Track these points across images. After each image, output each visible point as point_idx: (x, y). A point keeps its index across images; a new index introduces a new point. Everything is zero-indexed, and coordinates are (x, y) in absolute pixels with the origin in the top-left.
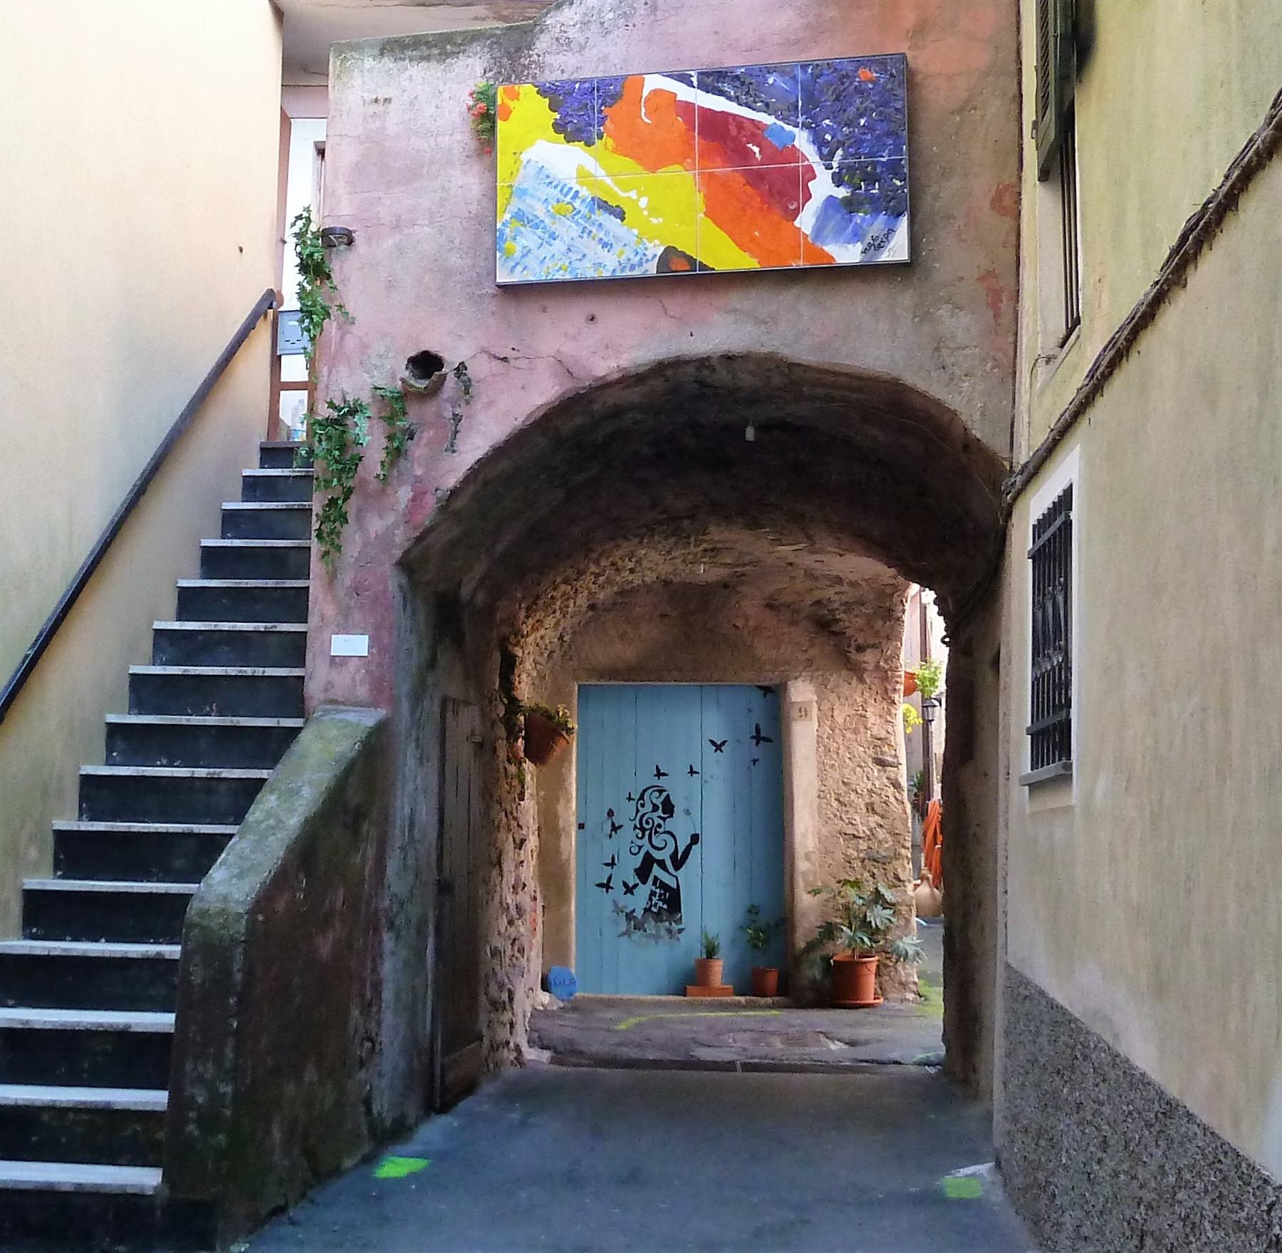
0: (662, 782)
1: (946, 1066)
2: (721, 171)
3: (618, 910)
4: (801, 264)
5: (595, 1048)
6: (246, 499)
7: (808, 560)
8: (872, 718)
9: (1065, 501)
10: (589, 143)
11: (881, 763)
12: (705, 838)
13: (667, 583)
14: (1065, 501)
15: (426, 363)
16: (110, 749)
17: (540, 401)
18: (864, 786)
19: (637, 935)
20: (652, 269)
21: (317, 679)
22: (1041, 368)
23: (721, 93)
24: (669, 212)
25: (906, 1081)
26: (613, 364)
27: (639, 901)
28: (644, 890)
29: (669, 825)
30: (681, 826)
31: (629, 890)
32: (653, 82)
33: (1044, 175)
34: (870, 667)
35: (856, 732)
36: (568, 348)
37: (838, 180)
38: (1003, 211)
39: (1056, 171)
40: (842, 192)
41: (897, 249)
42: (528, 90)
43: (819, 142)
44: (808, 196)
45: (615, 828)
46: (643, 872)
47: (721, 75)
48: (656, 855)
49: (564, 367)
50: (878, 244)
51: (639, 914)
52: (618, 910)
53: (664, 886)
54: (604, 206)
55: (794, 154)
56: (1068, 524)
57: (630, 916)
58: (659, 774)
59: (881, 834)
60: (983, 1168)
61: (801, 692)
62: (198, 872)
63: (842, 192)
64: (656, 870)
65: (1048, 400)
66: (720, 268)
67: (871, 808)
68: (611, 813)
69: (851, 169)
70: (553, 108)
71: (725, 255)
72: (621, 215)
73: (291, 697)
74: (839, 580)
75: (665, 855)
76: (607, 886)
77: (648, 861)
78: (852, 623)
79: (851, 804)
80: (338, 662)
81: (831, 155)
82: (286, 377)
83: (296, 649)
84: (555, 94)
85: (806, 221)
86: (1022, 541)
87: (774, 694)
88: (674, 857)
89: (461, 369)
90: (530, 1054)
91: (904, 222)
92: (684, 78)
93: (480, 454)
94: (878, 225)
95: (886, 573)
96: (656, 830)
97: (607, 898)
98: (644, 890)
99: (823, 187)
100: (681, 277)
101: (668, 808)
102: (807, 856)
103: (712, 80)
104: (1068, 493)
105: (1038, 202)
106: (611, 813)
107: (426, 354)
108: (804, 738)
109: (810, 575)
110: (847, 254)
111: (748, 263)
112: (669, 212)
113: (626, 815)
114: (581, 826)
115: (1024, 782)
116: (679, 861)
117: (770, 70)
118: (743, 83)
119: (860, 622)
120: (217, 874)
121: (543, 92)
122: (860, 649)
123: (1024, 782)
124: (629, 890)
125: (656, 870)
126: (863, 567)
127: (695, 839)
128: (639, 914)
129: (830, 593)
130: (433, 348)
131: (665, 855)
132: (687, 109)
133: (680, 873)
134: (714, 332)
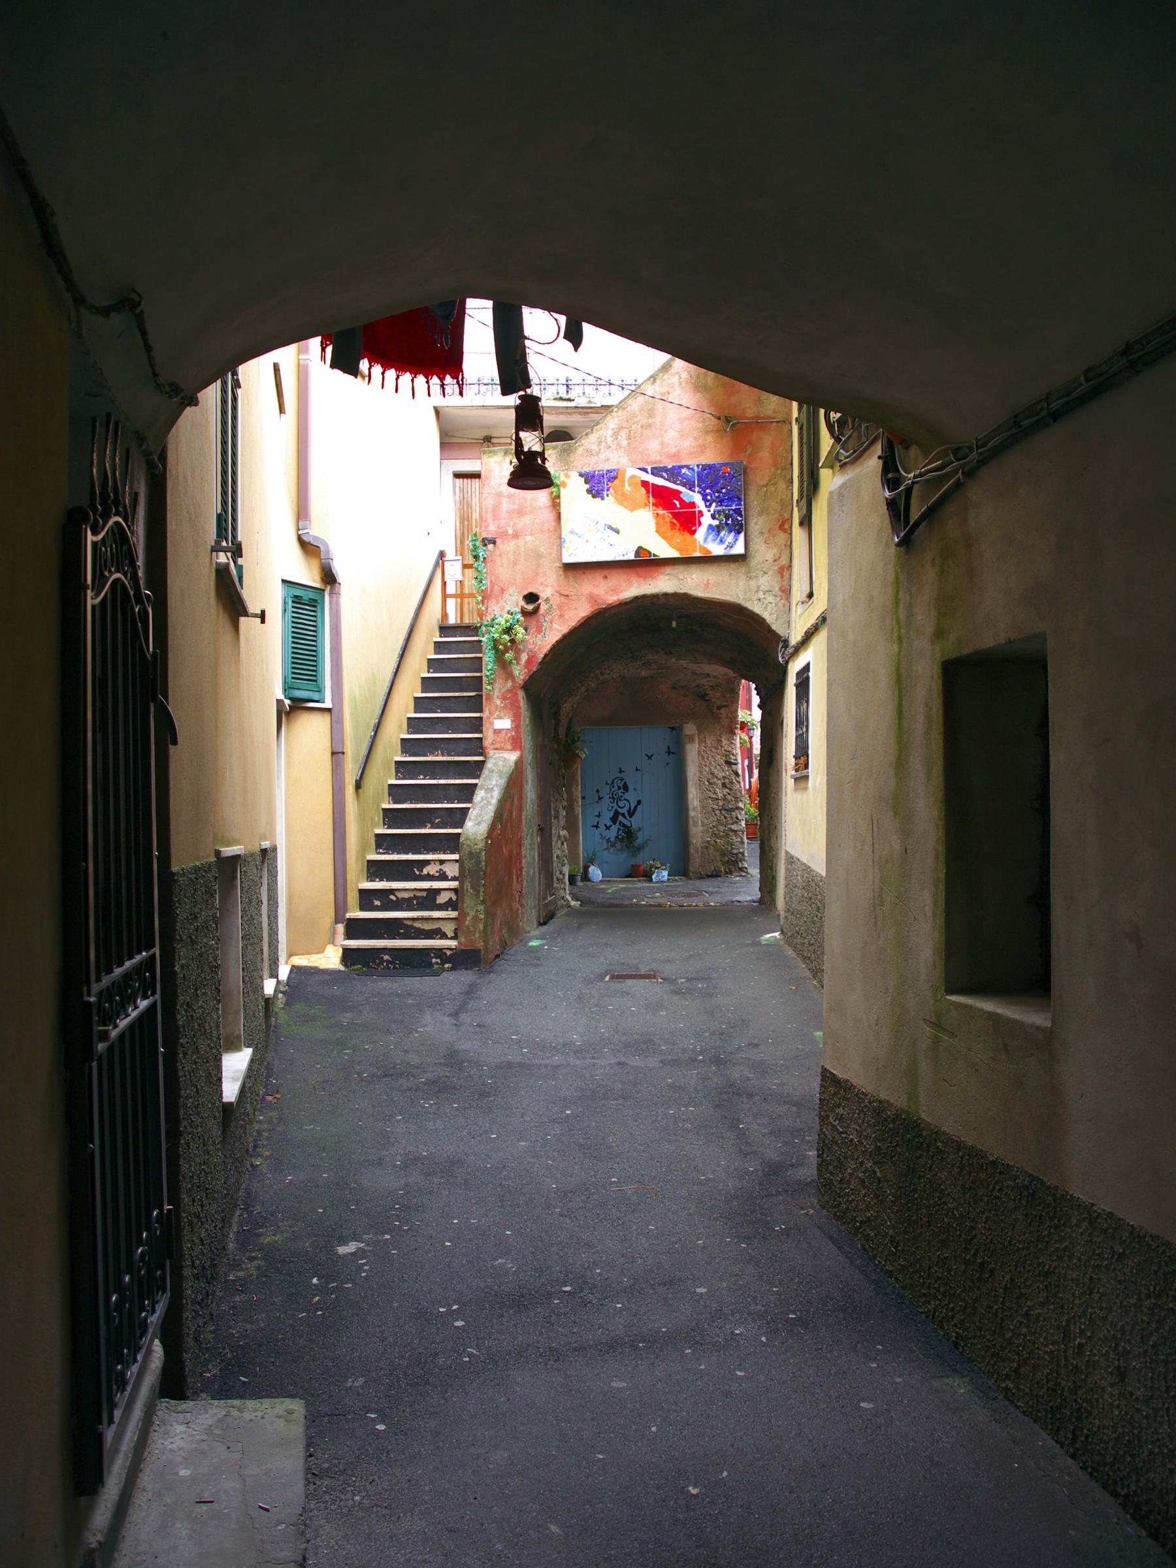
0: (622, 775)
1: (761, 901)
2: (661, 512)
3: (602, 837)
4: (697, 554)
5: (599, 900)
6: (436, 653)
7: (694, 667)
8: (724, 742)
9: (807, 668)
10: (603, 499)
11: (729, 763)
12: (643, 802)
13: (623, 677)
14: (807, 668)
15: (532, 598)
16: (397, 772)
17: (584, 614)
18: (721, 775)
19: (612, 850)
20: (631, 557)
21: (489, 738)
22: (799, 606)
23: (662, 477)
24: (639, 530)
25: (745, 907)
26: (615, 598)
27: (613, 833)
28: (614, 828)
29: (626, 796)
30: (633, 797)
31: (608, 828)
32: (631, 472)
33: (801, 524)
34: (724, 716)
35: (716, 748)
36: (595, 591)
37: (713, 517)
38: (785, 531)
39: (806, 523)
40: (716, 523)
41: (739, 549)
42: (574, 475)
43: (705, 500)
44: (700, 524)
45: (600, 798)
46: (614, 819)
47: (665, 469)
48: (620, 810)
49: (592, 598)
50: (731, 546)
51: (613, 839)
52: (602, 837)
53: (624, 826)
54: (610, 528)
55: (693, 505)
56: (808, 678)
57: (608, 841)
58: (621, 771)
59: (729, 797)
60: (777, 934)
61: (690, 729)
62: (460, 824)
63: (716, 523)
64: (620, 818)
65: (802, 622)
66: (662, 556)
67: (724, 785)
68: (598, 791)
69: (719, 512)
70: (586, 482)
71: (663, 549)
72: (617, 532)
73: (477, 746)
74: (708, 675)
75: (624, 811)
76: (597, 827)
77: (617, 814)
78: (715, 697)
79: (714, 784)
80: (497, 732)
81: (710, 506)
82: (448, 592)
83: (477, 724)
84: (588, 478)
85: (701, 533)
86: (792, 680)
87: (676, 730)
88: (629, 811)
89: (547, 600)
90: (573, 903)
91: (742, 536)
92: (645, 470)
93: (557, 638)
94: (730, 538)
95: (731, 673)
96: (619, 799)
97: (597, 832)
98: (614, 828)
99: (706, 520)
100: (644, 563)
101: (626, 788)
102: (694, 809)
103: (656, 472)
104: (808, 664)
105: (798, 533)
106: (598, 791)
107: (531, 594)
108: (692, 752)
109: (694, 673)
110: (717, 550)
111: (675, 554)
112: (639, 530)
113: (605, 791)
114: (583, 798)
115: (792, 776)
116: (631, 813)
117: (683, 467)
118: (673, 473)
119: (719, 694)
120: (469, 824)
121: (581, 475)
122: (719, 708)
123: (792, 776)
124: (608, 828)
125: (620, 818)
126: (717, 670)
127: (639, 802)
128: (613, 839)
129: (703, 681)
130: (534, 591)
131: (624, 811)
132: (645, 484)
133: (632, 819)
134: (663, 584)
